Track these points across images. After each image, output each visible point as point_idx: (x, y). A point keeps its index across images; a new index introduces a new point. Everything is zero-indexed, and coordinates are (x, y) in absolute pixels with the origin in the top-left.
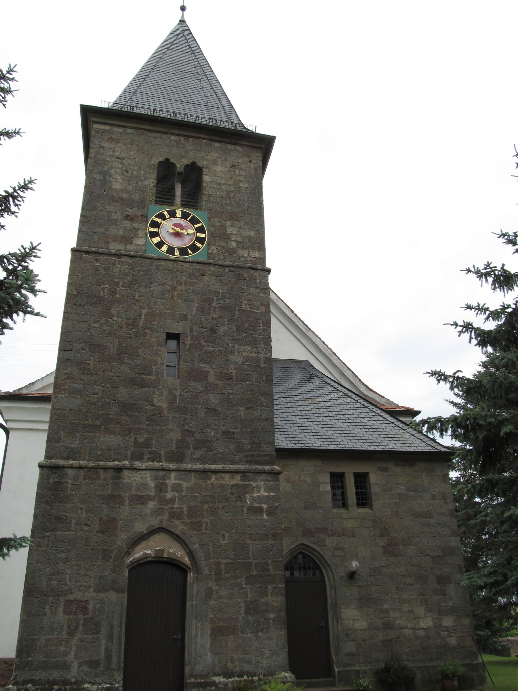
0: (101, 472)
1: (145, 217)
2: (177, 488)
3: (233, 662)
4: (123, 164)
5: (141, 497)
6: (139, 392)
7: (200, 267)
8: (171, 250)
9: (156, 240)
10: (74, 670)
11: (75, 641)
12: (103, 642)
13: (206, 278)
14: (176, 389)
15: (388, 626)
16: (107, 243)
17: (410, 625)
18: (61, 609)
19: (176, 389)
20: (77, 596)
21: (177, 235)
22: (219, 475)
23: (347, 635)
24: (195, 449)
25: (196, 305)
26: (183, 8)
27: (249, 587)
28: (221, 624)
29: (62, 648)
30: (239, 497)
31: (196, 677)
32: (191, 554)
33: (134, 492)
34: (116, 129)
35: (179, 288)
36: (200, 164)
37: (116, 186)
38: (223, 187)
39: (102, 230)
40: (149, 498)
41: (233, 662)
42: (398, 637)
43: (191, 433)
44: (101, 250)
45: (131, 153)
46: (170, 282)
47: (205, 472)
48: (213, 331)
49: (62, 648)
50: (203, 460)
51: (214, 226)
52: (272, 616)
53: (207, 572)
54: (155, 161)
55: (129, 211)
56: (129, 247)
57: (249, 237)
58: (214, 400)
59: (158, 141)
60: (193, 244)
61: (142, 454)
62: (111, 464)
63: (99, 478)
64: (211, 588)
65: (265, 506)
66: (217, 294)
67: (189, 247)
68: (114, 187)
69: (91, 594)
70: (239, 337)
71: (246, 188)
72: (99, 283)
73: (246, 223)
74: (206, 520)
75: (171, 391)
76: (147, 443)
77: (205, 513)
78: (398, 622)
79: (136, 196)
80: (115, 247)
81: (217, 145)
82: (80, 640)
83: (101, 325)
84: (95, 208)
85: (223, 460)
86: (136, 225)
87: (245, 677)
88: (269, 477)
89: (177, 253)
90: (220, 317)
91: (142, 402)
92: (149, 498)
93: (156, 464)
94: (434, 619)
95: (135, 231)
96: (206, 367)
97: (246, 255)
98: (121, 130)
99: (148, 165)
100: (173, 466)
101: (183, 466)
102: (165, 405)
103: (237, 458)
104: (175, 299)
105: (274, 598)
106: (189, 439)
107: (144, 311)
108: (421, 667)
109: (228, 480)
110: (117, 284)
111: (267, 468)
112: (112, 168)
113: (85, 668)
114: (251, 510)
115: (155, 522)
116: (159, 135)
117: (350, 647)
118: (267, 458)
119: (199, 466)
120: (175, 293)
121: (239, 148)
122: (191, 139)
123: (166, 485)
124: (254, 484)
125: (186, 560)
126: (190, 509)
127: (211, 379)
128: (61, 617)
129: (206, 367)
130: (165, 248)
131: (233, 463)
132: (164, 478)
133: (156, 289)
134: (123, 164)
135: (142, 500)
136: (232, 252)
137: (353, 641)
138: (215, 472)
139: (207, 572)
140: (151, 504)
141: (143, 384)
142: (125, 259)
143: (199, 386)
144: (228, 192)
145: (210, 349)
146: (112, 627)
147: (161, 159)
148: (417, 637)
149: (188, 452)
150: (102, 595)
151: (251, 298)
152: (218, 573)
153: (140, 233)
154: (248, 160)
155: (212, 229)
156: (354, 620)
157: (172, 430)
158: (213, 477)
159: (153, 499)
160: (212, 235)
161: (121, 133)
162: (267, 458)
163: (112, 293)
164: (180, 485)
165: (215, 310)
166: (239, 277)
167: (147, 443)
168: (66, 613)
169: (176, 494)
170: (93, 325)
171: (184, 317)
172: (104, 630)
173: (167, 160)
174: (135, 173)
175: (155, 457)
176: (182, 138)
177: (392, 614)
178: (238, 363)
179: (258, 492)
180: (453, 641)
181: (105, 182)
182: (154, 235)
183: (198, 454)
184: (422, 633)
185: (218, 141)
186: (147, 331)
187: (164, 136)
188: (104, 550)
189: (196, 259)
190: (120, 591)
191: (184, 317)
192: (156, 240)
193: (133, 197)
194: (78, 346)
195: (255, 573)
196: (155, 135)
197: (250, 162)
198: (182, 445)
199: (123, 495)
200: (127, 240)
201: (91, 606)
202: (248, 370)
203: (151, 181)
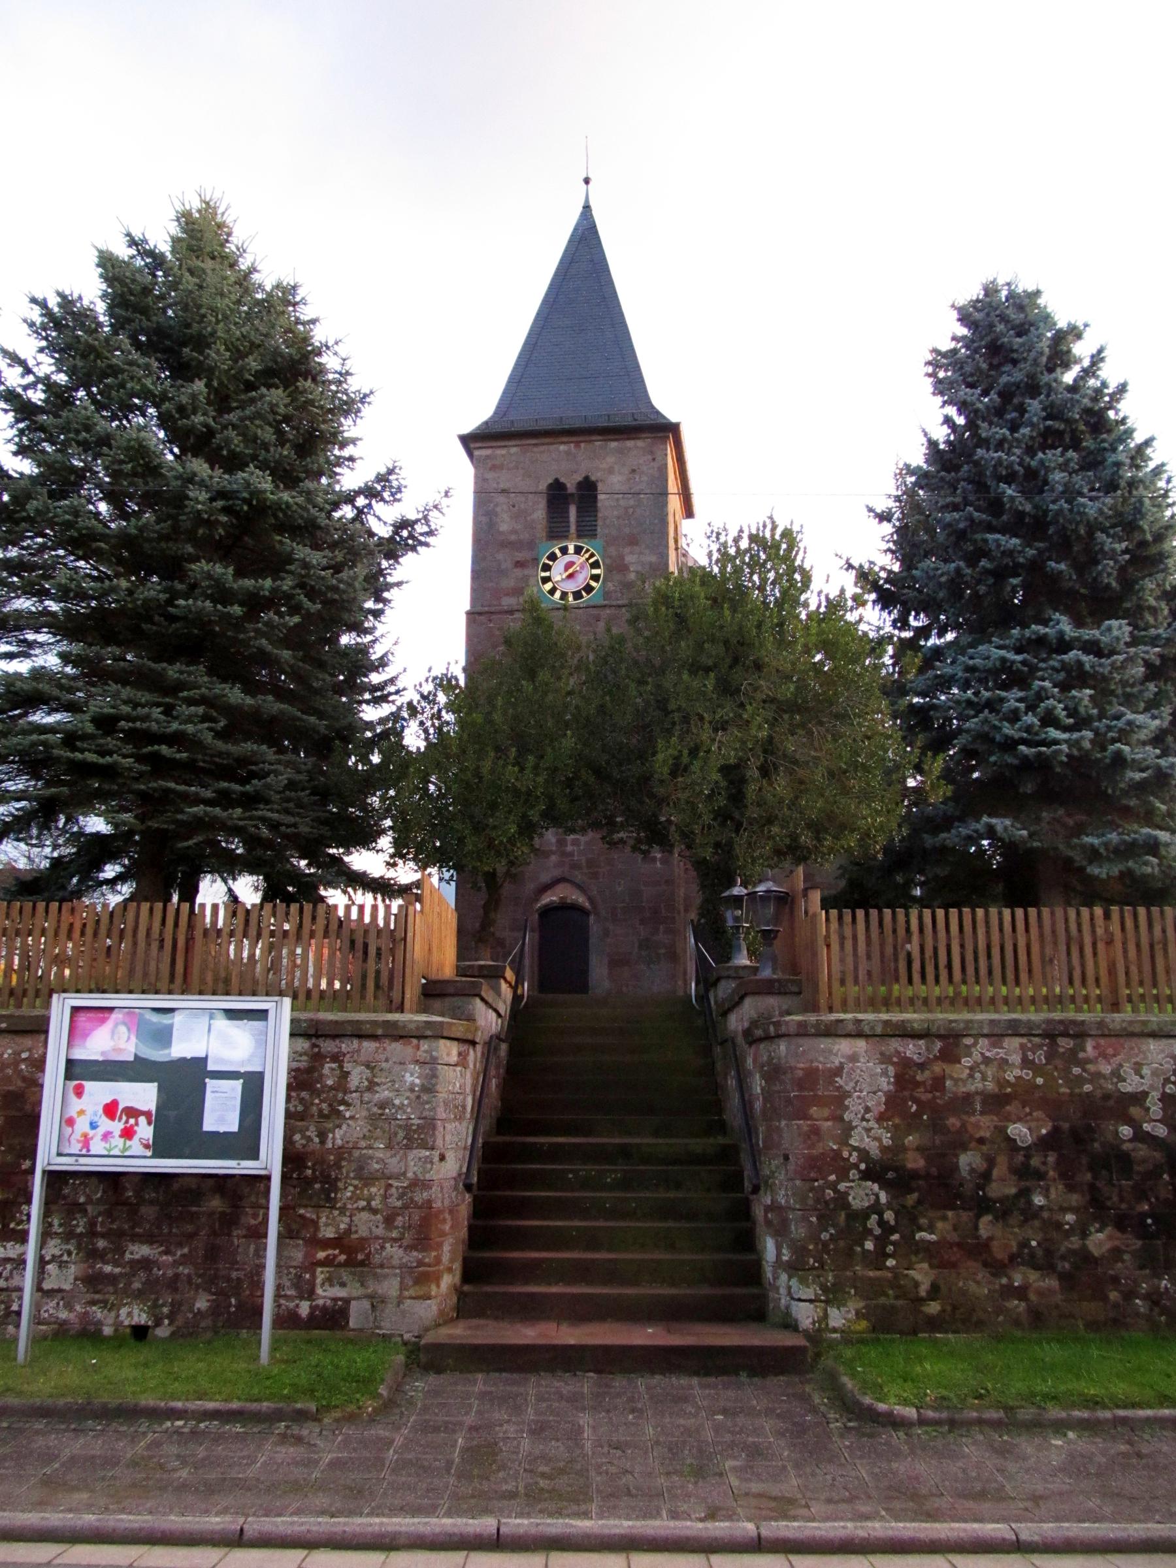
1: (536, 560)
7: (594, 612)
8: (564, 595)
9: (548, 586)
26: (587, 181)
32: (590, 899)
36: (593, 478)
37: (504, 527)
44: (493, 609)
51: (610, 557)
52: (662, 951)
54: (543, 486)
55: (520, 556)
60: (588, 585)
67: (584, 589)
79: (525, 536)
81: (614, 444)
86: (526, 572)
89: (571, 598)
95: (526, 579)
98: (503, 451)
99: (744, 743)
115: (557, 873)
121: (640, 443)
130: (558, 595)
140: (554, 858)
144: (626, 509)
147: (550, 481)
153: (532, 581)
154: (650, 457)
159: (553, 853)
160: (608, 570)
161: (503, 456)
176: (572, 445)
182: (546, 580)
189: (591, 603)
192: (548, 586)
193: (522, 537)
197: (654, 459)
203: (539, 513)
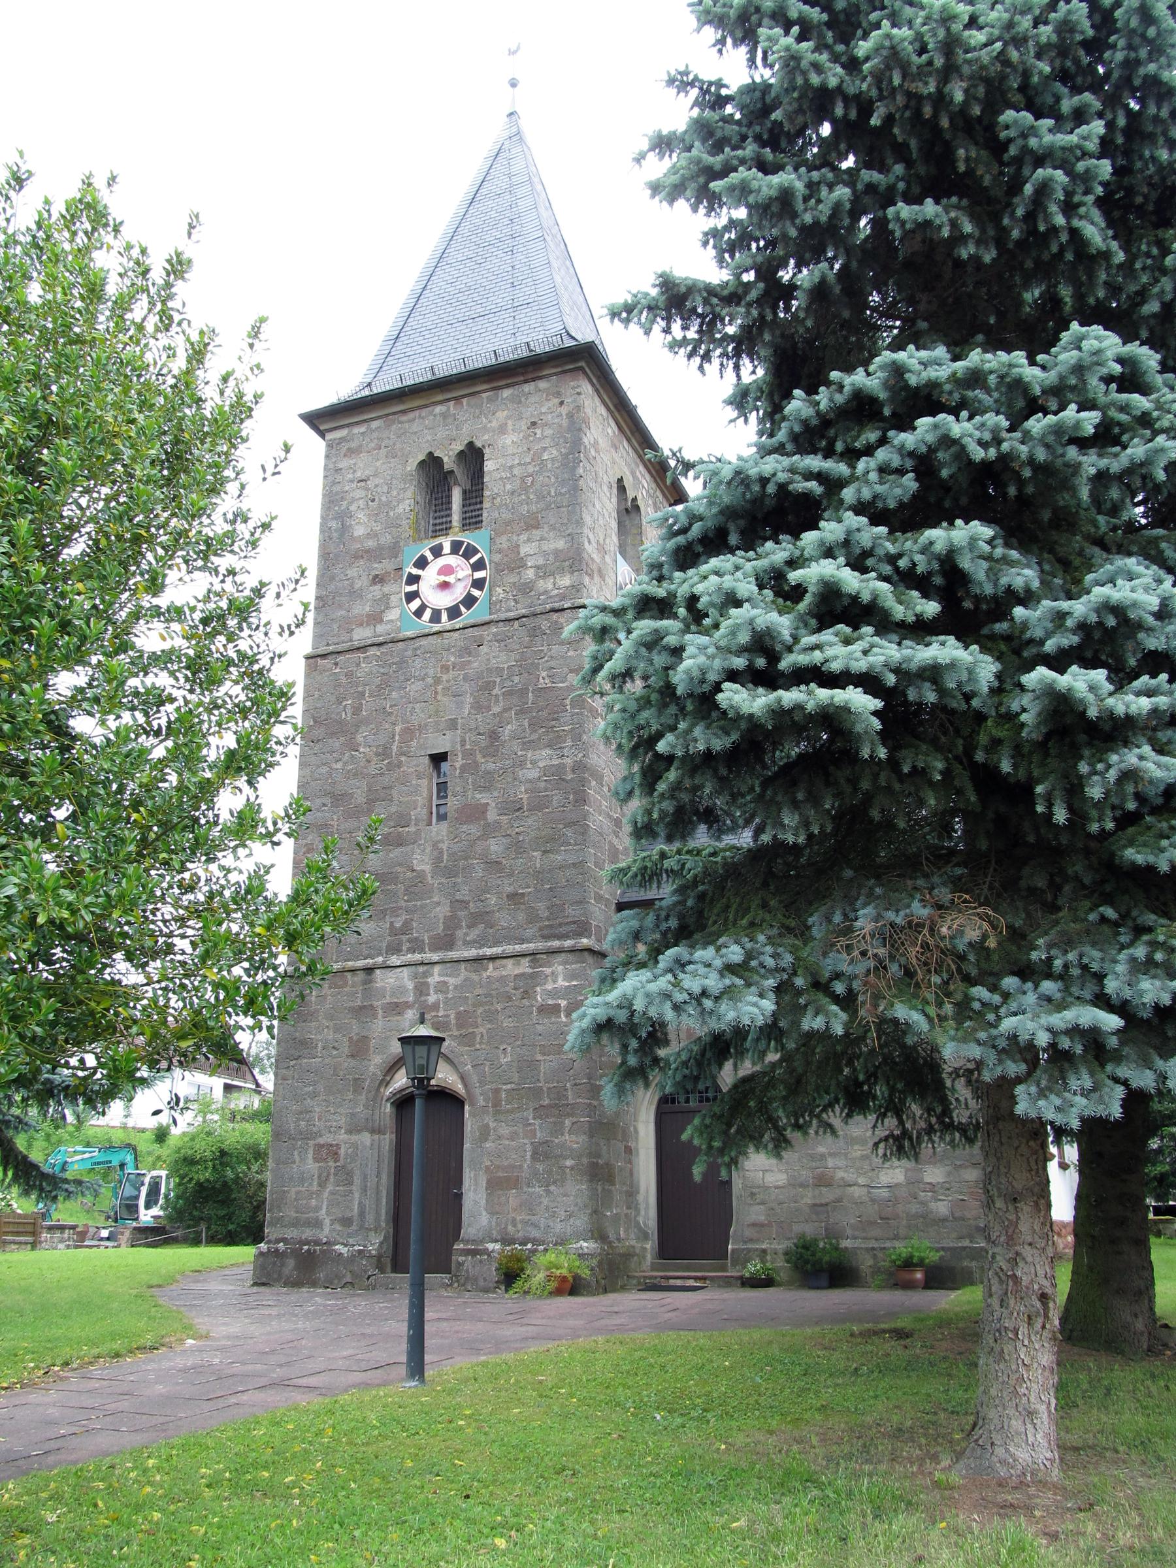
0: (349, 975)
2: (442, 987)
3: (515, 1226)
4: (367, 489)
5: (397, 1005)
6: (396, 853)
7: (474, 632)
10: (326, 1230)
11: (326, 1195)
12: (357, 1195)
13: (484, 649)
14: (442, 841)
15: (823, 1181)
16: (351, 631)
17: (861, 1180)
18: (310, 1155)
19: (442, 841)
20: (327, 1139)
21: (445, 586)
22: (498, 962)
23: (753, 1194)
24: (469, 927)
25: (469, 699)
27: (538, 1122)
28: (500, 1174)
29: (314, 1202)
30: (526, 992)
31: (467, 1242)
33: (388, 1000)
34: (356, 430)
35: (445, 677)
38: (516, 471)
39: (343, 613)
40: (407, 1006)
41: (515, 1226)
42: (839, 1200)
43: (464, 903)
44: (340, 648)
45: (378, 464)
46: (431, 672)
47: (477, 960)
48: (494, 736)
49: (314, 1202)
50: (480, 942)
52: (569, 1163)
53: (482, 1103)
54: (412, 465)
55: (379, 568)
56: (380, 629)
57: (557, 552)
58: (495, 847)
59: (415, 427)
61: (400, 943)
62: (360, 963)
63: (346, 983)
64: (487, 1125)
65: (563, 1003)
66: (499, 670)
68: (356, 534)
69: (343, 1136)
70: (534, 737)
71: (553, 460)
72: (339, 701)
73: (553, 528)
74: (481, 1029)
75: (435, 845)
76: (406, 928)
77: (479, 1020)
78: (840, 1174)
80: (362, 635)
81: (506, 393)
82: (332, 1193)
83: (345, 763)
84: (332, 578)
85: (510, 940)
87: (529, 1246)
88: (570, 957)
90: (506, 710)
91: (398, 869)
92: (407, 1006)
93: (417, 957)
94: (907, 1170)
96: (483, 798)
97: (550, 586)
98: (363, 429)
100: (435, 957)
101: (454, 955)
102: (427, 868)
103: (529, 933)
104: (439, 697)
105: (573, 1137)
106: (461, 914)
107: (398, 729)
108: (873, 1249)
109: (511, 968)
110: (363, 694)
111: (568, 943)
112: (353, 500)
113: (338, 1227)
114: (545, 1010)
116: (417, 413)
117: (757, 1214)
118: (574, 927)
119: (472, 953)
120: (440, 688)
121: (542, 384)
122: (465, 401)
123: (427, 984)
124: (548, 971)
125: (459, 1088)
126: (459, 1015)
127: (492, 815)
128: (311, 1166)
129: (483, 798)
131: (522, 941)
132: (425, 975)
133: (414, 688)
134: (367, 489)
135: (397, 1008)
136: (526, 589)
137: (763, 1203)
138: (492, 958)
139: (482, 1103)
141: (400, 842)
142: (373, 651)
143: (473, 830)
145: (491, 766)
146: (365, 1177)
147: (421, 457)
148: (873, 1200)
149: (460, 933)
150: (354, 1138)
151: (552, 664)
152: (496, 1104)
153: (394, 600)
154: (557, 401)
155: (497, 557)
156: (765, 1171)
157: (438, 904)
158: (491, 966)
160: (499, 569)
162: (574, 927)
163: (357, 710)
164: (445, 983)
165: (497, 701)
166: (535, 633)
167: (406, 928)
168: (316, 1160)
169: (441, 996)
170: (334, 766)
171: (453, 725)
172: (357, 1180)
173: (430, 454)
174: (384, 499)
175: (416, 947)
177: (831, 1162)
178: (530, 781)
179: (555, 982)
180: (941, 1208)
181: (344, 529)
182: (411, 597)
183: (473, 934)
184: (884, 1193)
185: (507, 386)
186: (403, 759)
187: (424, 412)
188: (356, 1080)
190: (376, 1131)
191: (453, 725)
193: (382, 541)
194: (318, 802)
195: (546, 1102)
196: (411, 415)
198: (452, 923)
199: (375, 1004)
200: (375, 618)
201: (342, 1152)
202: (546, 789)
